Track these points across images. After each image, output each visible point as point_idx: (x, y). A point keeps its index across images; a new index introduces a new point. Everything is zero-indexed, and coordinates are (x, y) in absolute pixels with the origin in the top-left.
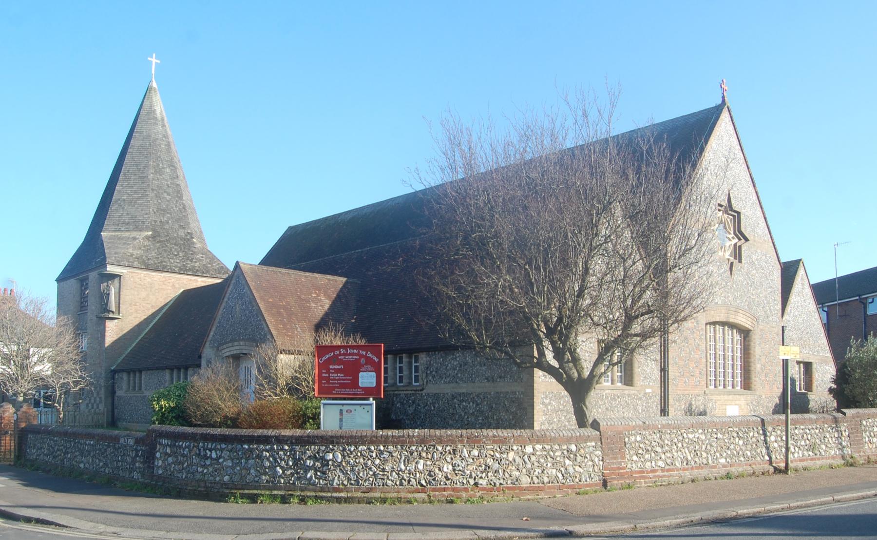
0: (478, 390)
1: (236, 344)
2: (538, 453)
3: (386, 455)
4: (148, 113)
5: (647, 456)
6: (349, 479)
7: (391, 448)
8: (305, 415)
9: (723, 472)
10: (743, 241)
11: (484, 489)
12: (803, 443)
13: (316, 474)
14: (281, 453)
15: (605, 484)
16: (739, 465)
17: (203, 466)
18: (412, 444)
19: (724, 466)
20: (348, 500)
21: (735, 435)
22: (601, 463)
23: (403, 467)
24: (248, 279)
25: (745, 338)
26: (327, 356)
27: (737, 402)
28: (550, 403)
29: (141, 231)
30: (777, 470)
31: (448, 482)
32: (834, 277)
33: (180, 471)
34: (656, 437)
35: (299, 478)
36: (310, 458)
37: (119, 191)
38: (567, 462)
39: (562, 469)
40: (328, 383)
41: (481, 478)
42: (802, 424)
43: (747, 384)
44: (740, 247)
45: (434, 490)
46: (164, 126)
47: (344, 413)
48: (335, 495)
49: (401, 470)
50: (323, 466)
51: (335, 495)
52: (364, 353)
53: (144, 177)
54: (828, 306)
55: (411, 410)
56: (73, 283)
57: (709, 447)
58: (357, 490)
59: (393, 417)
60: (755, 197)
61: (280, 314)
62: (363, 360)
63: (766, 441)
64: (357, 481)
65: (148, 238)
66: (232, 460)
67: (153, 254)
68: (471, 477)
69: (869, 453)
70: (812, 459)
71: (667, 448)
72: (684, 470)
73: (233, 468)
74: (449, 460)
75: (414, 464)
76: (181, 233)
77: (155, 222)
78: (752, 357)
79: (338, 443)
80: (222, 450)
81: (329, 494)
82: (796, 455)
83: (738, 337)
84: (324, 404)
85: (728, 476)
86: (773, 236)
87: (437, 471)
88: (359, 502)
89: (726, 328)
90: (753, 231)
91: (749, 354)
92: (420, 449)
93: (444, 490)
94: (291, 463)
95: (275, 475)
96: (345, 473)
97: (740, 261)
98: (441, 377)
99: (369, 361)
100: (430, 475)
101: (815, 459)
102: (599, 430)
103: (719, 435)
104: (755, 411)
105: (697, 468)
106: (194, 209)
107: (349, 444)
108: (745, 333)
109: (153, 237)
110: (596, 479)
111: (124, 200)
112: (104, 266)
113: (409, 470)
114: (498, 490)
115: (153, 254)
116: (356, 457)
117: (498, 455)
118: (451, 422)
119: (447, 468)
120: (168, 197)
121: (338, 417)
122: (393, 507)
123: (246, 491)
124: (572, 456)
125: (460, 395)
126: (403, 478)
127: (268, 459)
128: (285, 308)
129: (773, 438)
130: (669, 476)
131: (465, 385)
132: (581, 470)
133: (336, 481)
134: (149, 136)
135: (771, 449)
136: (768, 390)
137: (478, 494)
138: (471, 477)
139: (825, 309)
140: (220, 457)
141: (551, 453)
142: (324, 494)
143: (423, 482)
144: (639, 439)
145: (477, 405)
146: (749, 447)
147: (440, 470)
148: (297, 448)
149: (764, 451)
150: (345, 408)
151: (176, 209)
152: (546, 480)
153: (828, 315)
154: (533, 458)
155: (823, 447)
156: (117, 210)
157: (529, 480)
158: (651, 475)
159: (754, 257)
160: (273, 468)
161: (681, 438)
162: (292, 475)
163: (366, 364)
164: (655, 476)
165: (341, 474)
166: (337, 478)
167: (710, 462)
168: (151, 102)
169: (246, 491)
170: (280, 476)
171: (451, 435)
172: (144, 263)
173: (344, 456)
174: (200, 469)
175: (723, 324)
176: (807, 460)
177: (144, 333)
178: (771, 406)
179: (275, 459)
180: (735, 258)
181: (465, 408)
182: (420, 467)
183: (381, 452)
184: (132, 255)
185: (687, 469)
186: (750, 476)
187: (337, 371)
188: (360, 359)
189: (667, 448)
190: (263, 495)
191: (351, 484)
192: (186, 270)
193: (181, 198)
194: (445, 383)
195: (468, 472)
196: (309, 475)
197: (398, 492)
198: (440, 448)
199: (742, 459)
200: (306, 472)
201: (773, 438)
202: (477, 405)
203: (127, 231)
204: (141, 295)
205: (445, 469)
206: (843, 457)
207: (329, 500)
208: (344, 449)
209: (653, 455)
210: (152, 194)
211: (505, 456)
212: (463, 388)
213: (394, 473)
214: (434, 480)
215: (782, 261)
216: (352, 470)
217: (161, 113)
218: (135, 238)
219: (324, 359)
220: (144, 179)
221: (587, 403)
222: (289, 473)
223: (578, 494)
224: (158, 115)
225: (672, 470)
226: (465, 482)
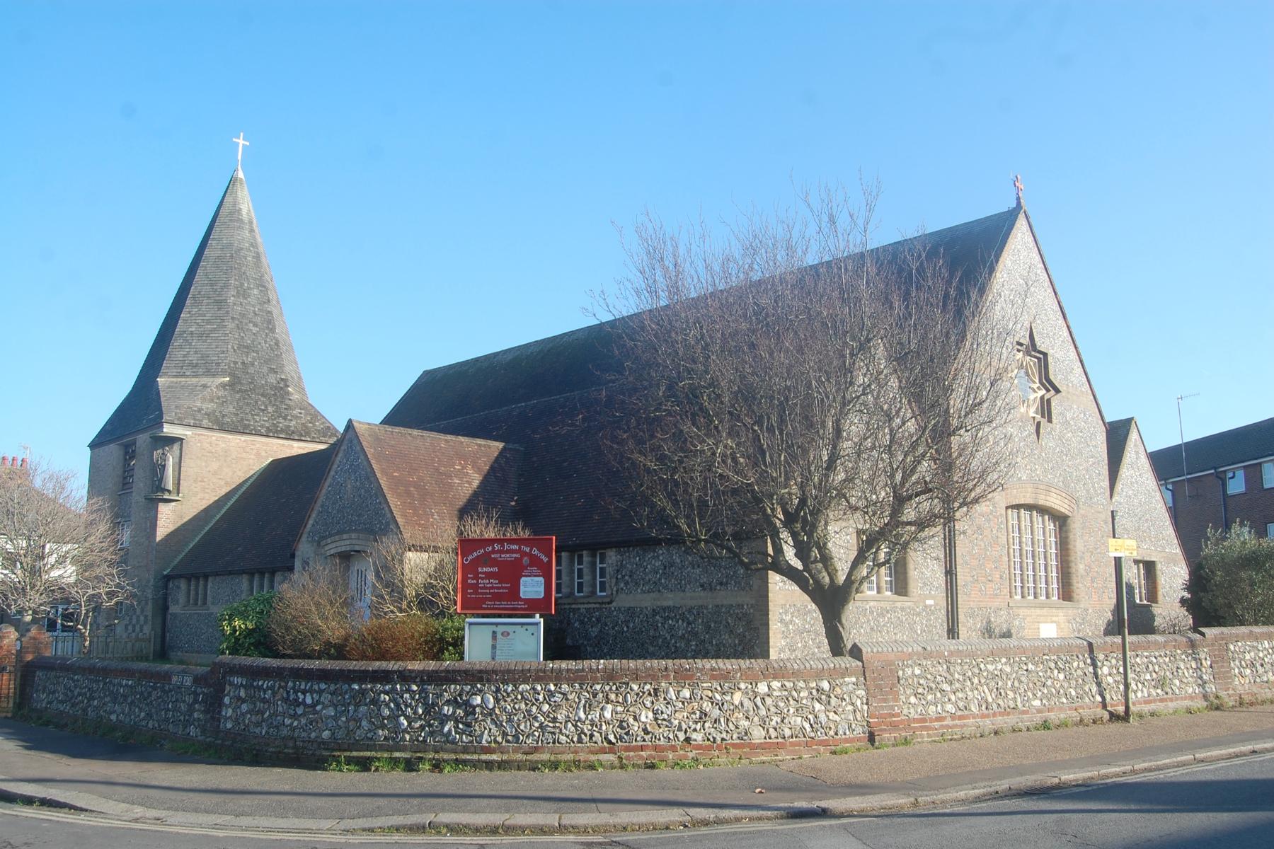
0: (690, 603)
1: (345, 536)
2: (775, 694)
3: (558, 698)
4: (230, 213)
6: (505, 734)
7: (565, 687)
8: (442, 639)
9: (1038, 719)
10: (1053, 392)
11: (699, 747)
12: (1148, 677)
13: (456, 727)
14: (407, 696)
15: (871, 738)
17: (291, 716)
19: (1039, 711)
20: (502, 765)
21: (1053, 665)
22: (865, 707)
23: (582, 716)
26: (475, 554)
28: (791, 621)
30: (1114, 717)
31: (647, 737)
32: (1177, 442)
33: (258, 724)
34: (942, 669)
35: (431, 734)
36: (448, 702)
37: (185, 321)
38: (818, 706)
40: (476, 592)
41: (695, 730)
42: (1145, 649)
43: (1067, 594)
44: (1049, 400)
45: (628, 749)
46: (252, 231)
47: (499, 636)
48: (484, 757)
49: (580, 720)
50: (467, 714)
51: (484, 757)
52: (527, 549)
53: (221, 301)
56: (113, 450)
57: (1016, 684)
58: (515, 751)
59: (569, 641)
60: (1066, 333)
61: (409, 494)
62: (526, 560)
63: (1096, 675)
64: (516, 737)
65: (223, 386)
66: (336, 706)
67: (231, 409)
68: (680, 729)
69: (1240, 690)
70: (1162, 700)
72: (983, 716)
73: (336, 718)
74: (648, 704)
75: (598, 710)
76: (272, 379)
77: (235, 363)
79: (489, 681)
80: (320, 692)
81: (475, 757)
84: (471, 624)
85: (1045, 726)
87: (631, 720)
88: (519, 769)
91: (1068, 549)
92: (607, 688)
95: (397, 729)
96: (499, 725)
97: (1050, 421)
99: (535, 561)
100: (622, 728)
103: (1030, 666)
104: (1079, 631)
105: (1001, 714)
106: (291, 345)
107: (505, 682)
108: (1061, 521)
110: (859, 731)
111: (192, 333)
112: (159, 423)
115: (231, 409)
117: (718, 697)
119: (646, 717)
120: (255, 330)
121: (490, 642)
122: (569, 774)
123: (355, 754)
124: (823, 697)
125: (664, 609)
127: (387, 705)
129: (1106, 670)
130: (962, 726)
132: (836, 718)
133: (486, 736)
134: (231, 245)
135: (1104, 685)
136: (1097, 602)
137: (691, 755)
138: (680, 729)
139: (1170, 487)
140: (318, 703)
141: (794, 693)
143: (612, 738)
144: (917, 672)
145: (689, 623)
146: (1073, 683)
147: (635, 719)
148: (430, 688)
149: (1094, 689)
150: (500, 629)
152: (787, 732)
154: (769, 701)
155: (1177, 682)
156: (180, 347)
158: (937, 724)
159: (1069, 415)
160: (394, 718)
162: (422, 728)
163: (530, 565)
164: (942, 727)
165: (493, 727)
166: (488, 733)
167: (1020, 705)
168: (235, 199)
169: (355, 754)
170: (405, 731)
171: (652, 668)
173: (497, 700)
174: (287, 721)
175: (1030, 507)
176: (1155, 701)
179: (398, 705)
180: (1043, 416)
181: (671, 628)
182: (608, 715)
183: (552, 694)
184: (200, 410)
185: (988, 716)
186: (1076, 724)
187: (489, 576)
188: (521, 559)
190: (378, 759)
191: (508, 741)
192: (277, 432)
193: (273, 330)
195: (676, 722)
196: (446, 729)
197: (576, 752)
198: (635, 687)
200: (442, 724)
201: (1106, 670)
202: (689, 623)
204: (211, 466)
205: (643, 719)
206: (1205, 697)
207: (475, 765)
208: (498, 690)
209: (939, 695)
211: (728, 698)
212: (670, 599)
213: (570, 725)
215: (1108, 420)
216: (510, 721)
218: (205, 386)
219: (470, 558)
220: (220, 304)
223: (834, 753)
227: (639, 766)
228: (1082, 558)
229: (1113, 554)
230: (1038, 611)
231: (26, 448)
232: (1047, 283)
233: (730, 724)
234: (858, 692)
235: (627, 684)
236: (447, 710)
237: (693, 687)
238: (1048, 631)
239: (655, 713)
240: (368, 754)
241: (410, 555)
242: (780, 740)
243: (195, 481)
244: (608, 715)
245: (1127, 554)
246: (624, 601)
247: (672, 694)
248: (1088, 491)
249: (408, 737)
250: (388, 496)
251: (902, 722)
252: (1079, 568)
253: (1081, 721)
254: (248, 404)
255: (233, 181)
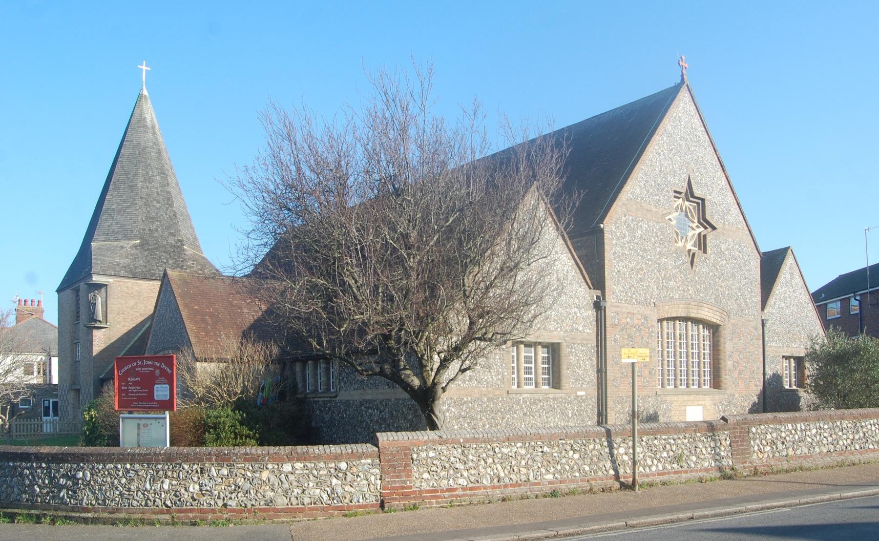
0: (381, 397)
2: (297, 472)
3: (132, 474)
4: (139, 121)
5: (442, 474)
6: (97, 499)
7: (137, 466)
8: (206, 424)
9: (548, 489)
10: (710, 229)
11: (233, 511)
12: (665, 454)
13: (68, 493)
14: (39, 471)
15: (382, 505)
16: (572, 481)
18: (158, 462)
19: (550, 483)
20: (94, 521)
21: (568, 448)
22: (379, 482)
23: (148, 486)
24: (173, 286)
25: (714, 334)
26: (126, 368)
27: (701, 402)
28: (448, 410)
29: (129, 240)
30: (624, 486)
31: (193, 503)
32: (865, 266)
34: (458, 452)
35: (53, 498)
36: (63, 476)
38: (334, 481)
39: (328, 489)
40: (127, 396)
41: (231, 498)
42: (665, 434)
43: (716, 383)
44: (705, 236)
45: (180, 511)
46: (154, 133)
47: (142, 427)
48: (83, 515)
49: (146, 490)
50: (73, 485)
51: (83, 515)
52: (158, 364)
53: (133, 186)
54: (860, 295)
55: (327, 417)
56: (68, 292)
57: (530, 462)
58: (104, 511)
59: (313, 424)
60: (724, 182)
61: (204, 321)
62: (157, 372)
63: (611, 454)
64: (104, 501)
65: (135, 246)
67: (141, 262)
68: (219, 498)
69: (757, 463)
70: (676, 473)
71: (471, 464)
72: (494, 487)
74: (195, 479)
75: (159, 483)
76: (171, 240)
77: (144, 230)
78: (722, 353)
79: (88, 461)
81: (78, 515)
82: (654, 469)
83: (707, 333)
84: (124, 418)
85: (554, 494)
86: (749, 223)
87: (183, 491)
88: (104, 524)
89: (690, 323)
90: (723, 218)
91: (718, 350)
92: (166, 467)
93: (191, 511)
94: (47, 482)
96: (94, 493)
97: (705, 252)
98: (351, 384)
100: (176, 495)
101: (680, 472)
102: (377, 446)
103: (545, 449)
104: (724, 411)
105: (512, 485)
106: (188, 216)
107: (98, 462)
108: (714, 329)
109: (141, 245)
110: (372, 500)
111: (113, 210)
112: (90, 276)
113: (155, 490)
114: (249, 511)
115: (141, 262)
116: (104, 476)
117: (249, 474)
118: (359, 430)
119: (194, 488)
120: (158, 205)
121: (136, 431)
122: (135, 528)
123: (9, 510)
124: (340, 475)
125: (366, 401)
126: (148, 499)
128: (211, 315)
129: (622, 450)
130: (471, 496)
131: (370, 392)
132: (352, 490)
133: (85, 500)
134: (139, 144)
135: (619, 462)
136: (743, 390)
137: (225, 516)
138: (219, 498)
139: (858, 298)
141: (315, 472)
142: (73, 514)
143: (168, 503)
144: (431, 454)
145: (381, 412)
146: (588, 461)
147: (186, 490)
148: (53, 466)
149: (609, 464)
150: (142, 422)
151: (166, 217)
152: (307, 500)
153: (860, 304)
154: (291, 477)
155: (694, 458)
157: (286, 501)
158: (447, 494)
159: (723, 247)
160: (31, 486)
161: (491, 453)
162: (48, 493)
163: (160, 376)
164: (452, 496)
165: (90, 494)
166: (87, 498)
167: (531, 478)
168: (142, 110)
169: (9, 510)
170: (38, 495)
171: (199, 453)
172: (131, 272)
173: (92, 474)
175: (686, 319)
176: (669, 473)
177: (133, 341)
178: (747, 405)
179: (34, 477)
180: (700, 249)
181: (371, 415)
182: (166, 487)
183: (128, 471)
184: (118, 264)
185: (499, 487)
186: (584, 492)
187: (135, 384)
188: (154, 371)
189: (471, 464)
190: (20, 514)
191: (99, 504)
193: (171, 205)
194: (354, 389)
195: (216, 493)
196: (61, 495)
197: (143, 513)
198: (186, 467)
199: (577, 474)
200: (60, 491)
201: (622, 450)
202: (381, 412)
203: (116, 240)
204: (126, 305)
205: (191, 489)
206: (720, 469)
207: (78, 520)
208: (93, 467)
209: (451, 472)
210: (140, 203)
211: (257, 475)
213: (140, 493)
214: (179, 500)
215: (762, 251)
216: (100, 489)
217: (152, 121)
218: (122, 247)
219: (123, 371)
220: (132, 187)
221: (437, 412)
222: (45, 491)
223: (345, 516)
224: (149, 124)
225: (478, 488)
226: (212, 503)
227: (186, 524)
228: (730, 356)
229: (625, 360)
230: (686, 397)
231: (40, 293)
232: (708, 143)
233: (259, 494)
234: (373, 471)
235: (180, 464)
236: (62, 481)
237: (230, 466)
238: (695, 414)
239: (201, 485)
240: (16, 511)
241: (198, 364)
242: (300, 506)
243: (118, 314)
244: (166, 487)
245: (640, 360)
246: (343, 396)
247: (214, 472)
248: (739, 305)
249: (39, 500)
250: (186, 323)
251: (414, 492)
252: (728, 364)
253: (591, 490)
254: (154, 259)
255: (140, 97)
